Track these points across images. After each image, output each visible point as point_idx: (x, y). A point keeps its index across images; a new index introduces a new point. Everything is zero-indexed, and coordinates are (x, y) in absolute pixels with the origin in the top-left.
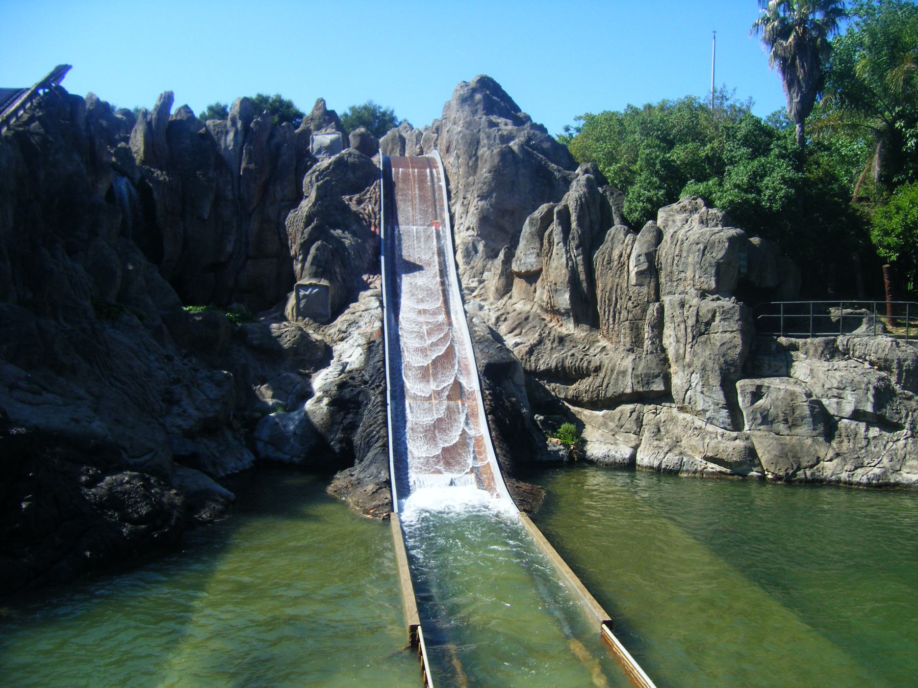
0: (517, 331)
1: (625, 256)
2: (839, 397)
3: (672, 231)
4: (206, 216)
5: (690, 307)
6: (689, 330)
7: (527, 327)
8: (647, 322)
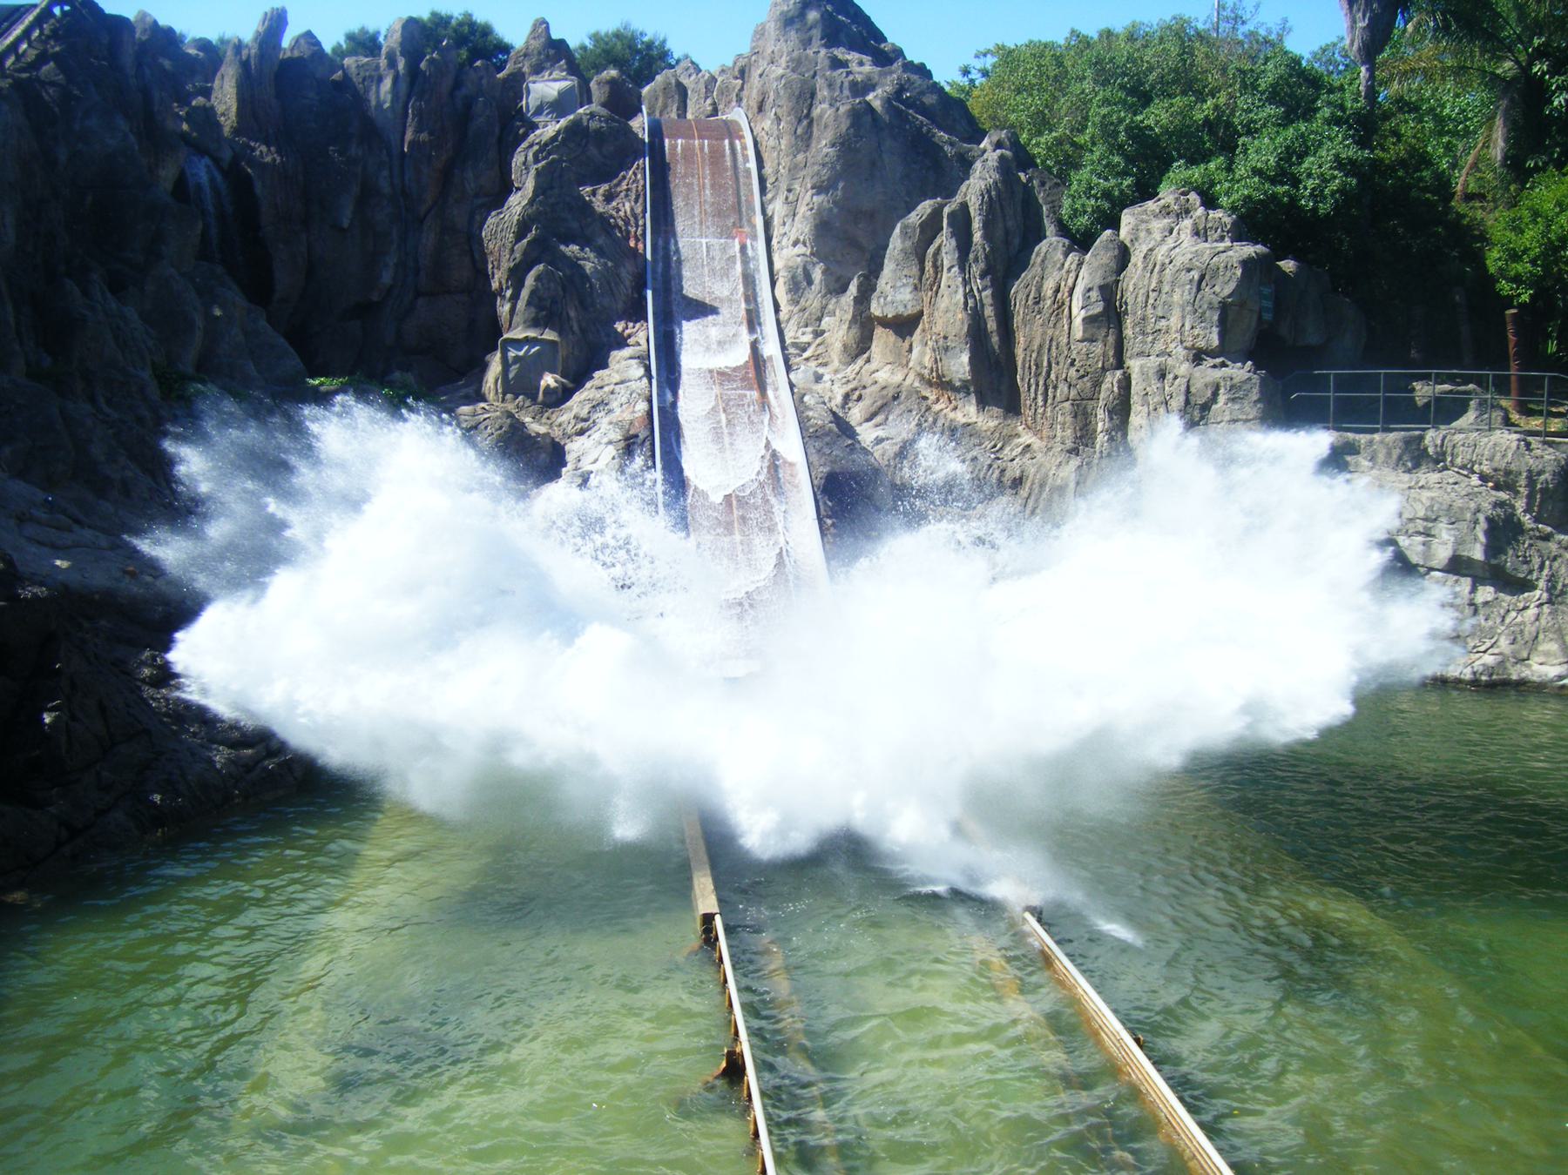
0: (879, 419)
1: (1064, 290)
2: (1427, 533)
3: (1145, 249)
4: (346, 223)
5: (1176, 378)
8: (1101, 403)
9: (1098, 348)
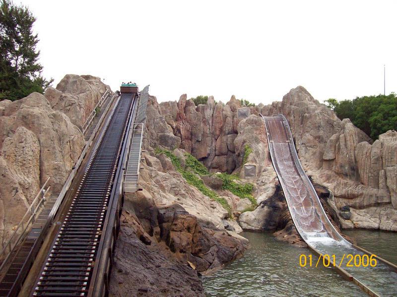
7: (331, 180)
9: (377, 165)
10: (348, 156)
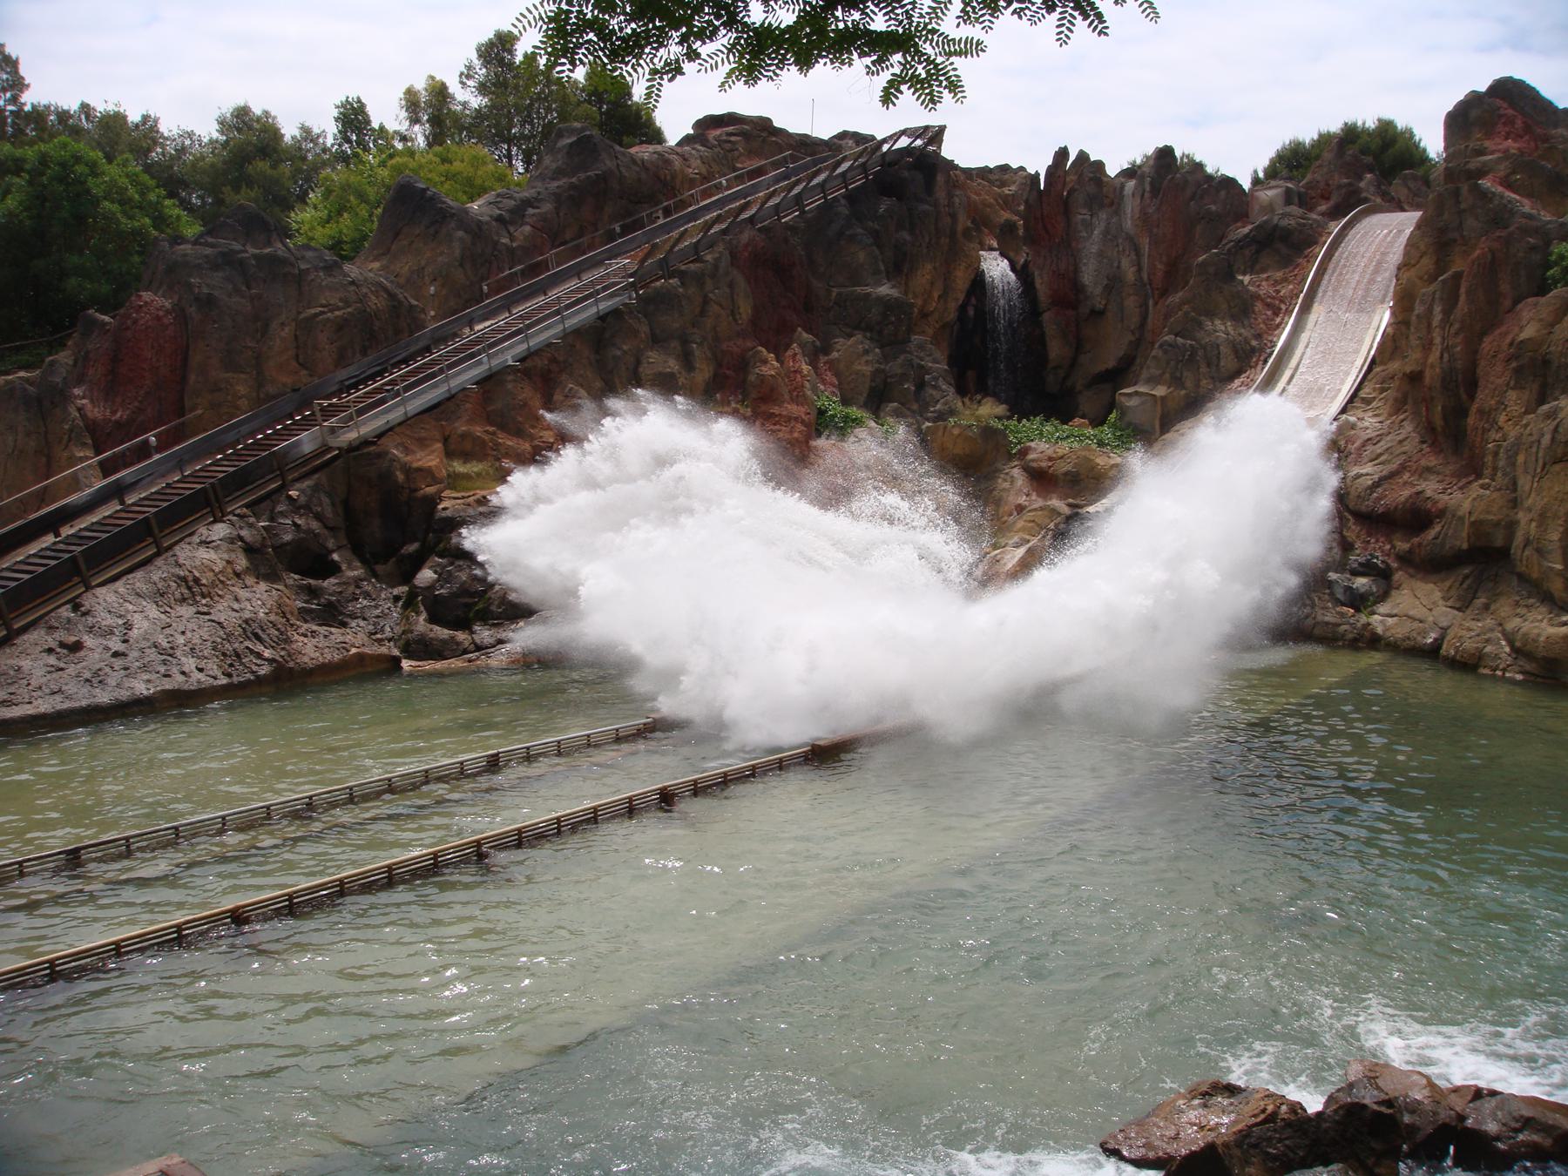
6: (1540, 455)
10: (1446, 355)
